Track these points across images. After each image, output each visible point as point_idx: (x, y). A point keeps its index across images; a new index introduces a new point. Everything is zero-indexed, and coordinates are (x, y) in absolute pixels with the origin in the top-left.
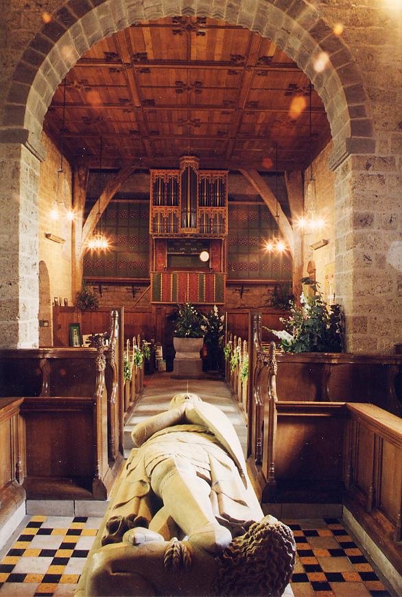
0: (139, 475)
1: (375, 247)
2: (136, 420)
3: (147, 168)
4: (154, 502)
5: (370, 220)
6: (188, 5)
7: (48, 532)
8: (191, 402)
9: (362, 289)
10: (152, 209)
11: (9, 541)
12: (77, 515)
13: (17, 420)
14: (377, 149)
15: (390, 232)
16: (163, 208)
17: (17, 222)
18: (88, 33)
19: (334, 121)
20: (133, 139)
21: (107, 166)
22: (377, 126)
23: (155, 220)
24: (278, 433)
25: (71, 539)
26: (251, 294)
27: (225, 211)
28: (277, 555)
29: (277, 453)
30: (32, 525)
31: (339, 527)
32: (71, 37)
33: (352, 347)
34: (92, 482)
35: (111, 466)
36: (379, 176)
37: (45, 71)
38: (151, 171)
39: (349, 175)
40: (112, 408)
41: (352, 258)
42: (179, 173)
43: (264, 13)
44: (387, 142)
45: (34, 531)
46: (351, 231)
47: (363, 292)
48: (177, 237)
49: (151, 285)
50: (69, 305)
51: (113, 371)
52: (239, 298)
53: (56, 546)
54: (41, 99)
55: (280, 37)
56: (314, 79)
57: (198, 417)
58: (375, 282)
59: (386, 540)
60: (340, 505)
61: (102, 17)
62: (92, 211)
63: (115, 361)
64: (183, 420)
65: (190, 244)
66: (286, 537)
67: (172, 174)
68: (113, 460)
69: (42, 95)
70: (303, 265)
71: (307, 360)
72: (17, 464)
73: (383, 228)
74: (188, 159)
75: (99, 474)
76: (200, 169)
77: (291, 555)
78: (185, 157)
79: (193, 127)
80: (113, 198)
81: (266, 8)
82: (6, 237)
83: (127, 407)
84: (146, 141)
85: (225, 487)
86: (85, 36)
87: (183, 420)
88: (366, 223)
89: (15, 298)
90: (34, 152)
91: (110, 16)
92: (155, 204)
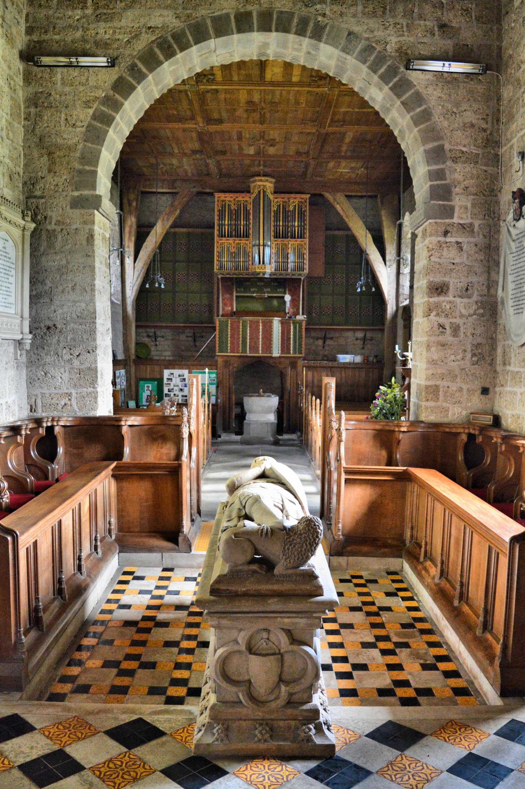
1: (449, 316)
3: (211, 191)
5: (445, 288)
6: (263, 51)
9: (435, 357)
10: (218, 242)
12: (165, 566)
13: (109, 482)
14: (456, 215)
15: (466, 300)
16: (231, 241)
17: (93, 290)
18: (157, 85)
22: (457, 190)
24: (345, 495)
26: (336, 343)
27: (305, 244)
30: (125, 573)
33: (424, 415)
36: (458, 243)
38: (217, 195)
42: (250, 198)
43: (344, 63)
47: (437, 361)
48: (246, 276)
49: (217, 332)
52: (320, 348)
58: (449, 351)
62: (145, 244)
64: (263, 476)
65: (263, 283)
67: (241, 198)
69: (111, 154)
73: (460, 296)
74: (261, 181)
76: (275, 192)
78: (257, 178)
79: (267, 147)
80: (172, 227)
81: (346, 59)
82: (83, 305)
84: (209, 161)
87: (263, 476)
88: (442, 291)
89: (93, 366)
90: (106, 215)
91: (181, 66)
92: (221, 236)
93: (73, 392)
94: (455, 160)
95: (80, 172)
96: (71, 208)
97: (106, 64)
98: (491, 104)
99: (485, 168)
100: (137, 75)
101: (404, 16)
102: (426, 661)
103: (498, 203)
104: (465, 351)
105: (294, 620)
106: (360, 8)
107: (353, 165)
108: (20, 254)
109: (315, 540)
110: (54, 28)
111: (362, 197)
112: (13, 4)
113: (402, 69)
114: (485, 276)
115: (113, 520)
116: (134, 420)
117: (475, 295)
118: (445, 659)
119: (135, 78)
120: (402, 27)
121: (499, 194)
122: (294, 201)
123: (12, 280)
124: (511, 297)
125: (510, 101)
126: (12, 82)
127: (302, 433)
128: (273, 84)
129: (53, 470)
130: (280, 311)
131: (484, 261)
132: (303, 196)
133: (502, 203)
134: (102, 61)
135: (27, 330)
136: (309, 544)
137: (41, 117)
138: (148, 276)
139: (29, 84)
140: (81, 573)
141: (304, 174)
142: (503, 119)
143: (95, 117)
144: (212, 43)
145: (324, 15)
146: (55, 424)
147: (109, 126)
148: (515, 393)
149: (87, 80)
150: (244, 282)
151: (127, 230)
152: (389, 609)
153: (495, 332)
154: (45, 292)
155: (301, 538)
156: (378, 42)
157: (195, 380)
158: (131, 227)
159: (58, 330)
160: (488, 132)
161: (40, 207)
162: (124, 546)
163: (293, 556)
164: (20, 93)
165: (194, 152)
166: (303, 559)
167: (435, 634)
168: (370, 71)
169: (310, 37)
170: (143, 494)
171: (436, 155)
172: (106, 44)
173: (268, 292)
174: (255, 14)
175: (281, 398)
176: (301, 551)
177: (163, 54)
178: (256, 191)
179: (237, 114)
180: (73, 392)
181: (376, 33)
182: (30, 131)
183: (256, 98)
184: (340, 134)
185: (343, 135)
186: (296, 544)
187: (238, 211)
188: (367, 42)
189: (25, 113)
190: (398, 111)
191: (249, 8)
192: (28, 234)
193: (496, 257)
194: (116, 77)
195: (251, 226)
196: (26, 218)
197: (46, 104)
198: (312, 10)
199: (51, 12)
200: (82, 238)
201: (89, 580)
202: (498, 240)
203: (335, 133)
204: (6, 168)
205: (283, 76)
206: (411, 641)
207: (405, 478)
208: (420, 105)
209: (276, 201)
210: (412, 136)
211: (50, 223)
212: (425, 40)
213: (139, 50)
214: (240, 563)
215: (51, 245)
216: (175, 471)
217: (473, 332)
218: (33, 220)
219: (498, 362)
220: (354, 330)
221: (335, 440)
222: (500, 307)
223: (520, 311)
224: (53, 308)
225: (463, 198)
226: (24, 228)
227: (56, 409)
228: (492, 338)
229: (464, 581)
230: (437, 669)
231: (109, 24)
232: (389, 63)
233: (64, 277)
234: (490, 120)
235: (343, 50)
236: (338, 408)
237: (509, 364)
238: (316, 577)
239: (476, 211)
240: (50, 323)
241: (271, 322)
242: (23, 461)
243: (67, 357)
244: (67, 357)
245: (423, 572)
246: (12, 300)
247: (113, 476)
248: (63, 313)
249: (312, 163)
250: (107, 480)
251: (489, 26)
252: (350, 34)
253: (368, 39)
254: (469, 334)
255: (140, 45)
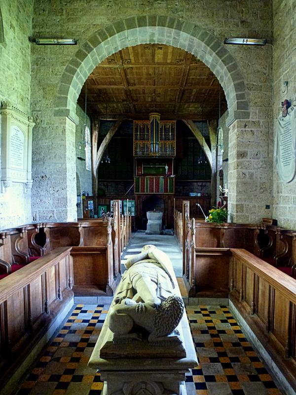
0: (127, 281)
2: (126, 257)
4: (134, 291)
5: (245, 154)
6: (152, 38)
7: (85, 312)
8: (151, 249)
11: (71, 310)
15: (256, 160)
17: (65, 157)
18: (99, 55)
19: (229, 100)
20: (123, 104)
21: (110, 118)
22: (251, 104)
23: (136, 148)
25: (97, 315)
28: (176, 308)
29: (196, 271)
30: (77, 309)
31: (226, 310)
32: (90, 58)
34: (106, 287)
35: (115, 280)
36: (251, 131)
37: (77, 77)
39: (236, 130)
40: (115, 251)
41: (236, 174)
44: (256, 113)
45: (78, 311)
46: (236, 160)
49: (135, 184)
50: (90, 195)
51: (115, 232)
53: (90, 318)
54: (75, 92)
55: (201, 54)
56: (219, 77)
57: (153, 256)
59: (247, 315)
60: (227, 299)
61: (106, 46)
63: (116, 228)
64: (147, 257)
66: (180, 301)
68: (116, 277)
69: (76, 90)
70: (217, 172)
71: (213, 226)
72: (69, 279)
73: (253, 158)
74: (154, 114)
75: (109, 283)
77: (182, 308)
82: (60, 165)
83: (123, 250)
85: (163, 286)
86: (97, 57)
87: (147, 257)
88: (244, 156)
93: (55, 210)
94: (249, 89)
95: (59, 98)
96: (54, 116)
97: (72, 43)
98: (268, 60)
99: (266, 93)
100: (88, 49)
101: (223, 17)
102: (251, 373)
103: (272, 110)
104: (256, 186)
105: (164, 376)
106: (201, 13)
107: (196, 106)
108: (27, 139)
109: (179, 315)
110: (47, 25)
111: (199, 122)
112: (24, 11)
113: (223, 44)
114: (266, 147)
115: (72, 279)
116: (85, 224)
117: (261, 157)
118: (231, 318)
119: (87, 50)
120: (222, 22)
121: (273, 106)
122: (169, 124)
123: (22, 152)
124: (281, 157)
125: (278, 58)
126: (24, 52)
127: (174, 229)
128: (159, 64)
129: (43, 251)
130: (163, 174)
131: (266, 140)
132: (174, 121)
133: (274, 110)
134: (70, 41)
135: (30, 177)
136: (174, 318)
137: (40, 70)
138: (103, 158)
139: (34, 53)
140: (47, 313)
141: (173, 111)
142: (274, 67)
143: (66, 70)
144: (126, 32)
145: (182, 17)
146: (44, 226)
147: (74, 74)
148: (286, 208)
149: (63, 51)
150: (148, 161)
151: (94, 137)
152: (223, 332)
153: (272, 176)
154: (41, 159)
155: (168, 314)
156: (210, 30)
157: (117, 203)
158: (96, 136)
159: (47, 178)
160: (267, 75)
161: (39, 116)
162: (77, 294)
163: (162, 327)
164: (29, 58)
165: (123, 101)
166: (170, 329)
167: (254, 351)
168: (206, 45)
169: (175, 29)
170: (87, 264)
171: (239, 87)
172: (73, 33)
173: (158, 165)
174: (147, 17)
175: (164, 213)
176: (168, 323)
177: (101, 38)
178: (152, 119)
179: (142, 80)
180: (55, 210)
181: (209, 26)
182: (34, 77)
183: (151, 71)
184: (190, 90)
185: (191, 90)
186: (164, 318)
187: (144, 129)
188: (204, 31)
189: (31, 68)
190: (220, 65)
191: (144, 14)
192: (31, 129)
193: (272, 138)
194: (77, 50)
195: (150, 135)
196: (30, 120)
197: (42, 64)
198: (176, 15)
199: (45, 18)
200: (60, 131)
201: (51, 316)
202: (272, 129)
203: (188, 90)
204: (19, 94)
205: (163, 60)
206: (240, 356)
207: (229, 254)
208: (232, 62)
209: (161, 124)
210: (227, 78)
211: (44, 124)
212: (234, 29)
213: (89, 37)
214: (122, 333)
215: (44, 135)
216: (104, 251)
217: (261, 176)
218: (34, 121)
219: (274, 192)
220: (197, 182)
221: (190, 233)
222: (275, 163)
223: (288, 164)
224: (45, 167)
225: (254, 108)
226: (29, 126)
227: (46, 219)
228: (270, 180)
229: (271, 319)
230: (259, 380)
231: (74, 23)
232: (215, 41)
233: (51, 151)
234: (267, 69)
235: (192, 35)
236: (191, 217)
237: (281, 193)
238: (181, 343)
239: (261, 114)
240: (43, 175)
241: (159, 178)
242: (27, 246)
243: (52, 192)
244: (52, 192)
245: (242, 309)
246: (22, 162)
247: (71, 254)
248: (50, 169)
249: (178, 105)
250: (68, 256)
251: (267, 21)
252: (195, 26)
253: (205, 29)
254: (258, 178)
255: (90, 34)
